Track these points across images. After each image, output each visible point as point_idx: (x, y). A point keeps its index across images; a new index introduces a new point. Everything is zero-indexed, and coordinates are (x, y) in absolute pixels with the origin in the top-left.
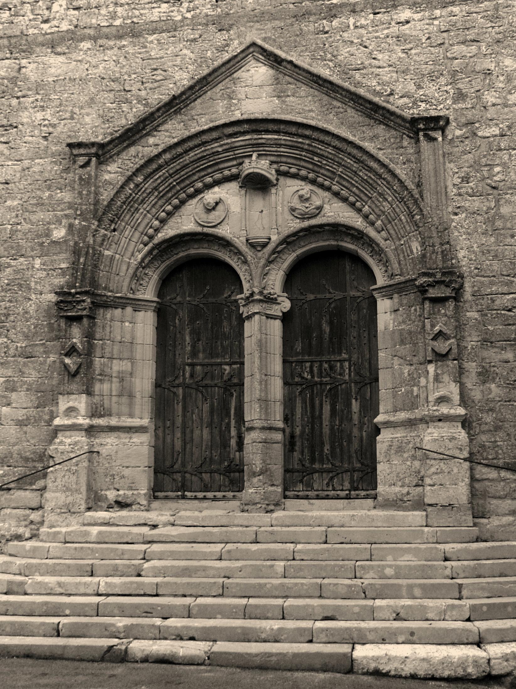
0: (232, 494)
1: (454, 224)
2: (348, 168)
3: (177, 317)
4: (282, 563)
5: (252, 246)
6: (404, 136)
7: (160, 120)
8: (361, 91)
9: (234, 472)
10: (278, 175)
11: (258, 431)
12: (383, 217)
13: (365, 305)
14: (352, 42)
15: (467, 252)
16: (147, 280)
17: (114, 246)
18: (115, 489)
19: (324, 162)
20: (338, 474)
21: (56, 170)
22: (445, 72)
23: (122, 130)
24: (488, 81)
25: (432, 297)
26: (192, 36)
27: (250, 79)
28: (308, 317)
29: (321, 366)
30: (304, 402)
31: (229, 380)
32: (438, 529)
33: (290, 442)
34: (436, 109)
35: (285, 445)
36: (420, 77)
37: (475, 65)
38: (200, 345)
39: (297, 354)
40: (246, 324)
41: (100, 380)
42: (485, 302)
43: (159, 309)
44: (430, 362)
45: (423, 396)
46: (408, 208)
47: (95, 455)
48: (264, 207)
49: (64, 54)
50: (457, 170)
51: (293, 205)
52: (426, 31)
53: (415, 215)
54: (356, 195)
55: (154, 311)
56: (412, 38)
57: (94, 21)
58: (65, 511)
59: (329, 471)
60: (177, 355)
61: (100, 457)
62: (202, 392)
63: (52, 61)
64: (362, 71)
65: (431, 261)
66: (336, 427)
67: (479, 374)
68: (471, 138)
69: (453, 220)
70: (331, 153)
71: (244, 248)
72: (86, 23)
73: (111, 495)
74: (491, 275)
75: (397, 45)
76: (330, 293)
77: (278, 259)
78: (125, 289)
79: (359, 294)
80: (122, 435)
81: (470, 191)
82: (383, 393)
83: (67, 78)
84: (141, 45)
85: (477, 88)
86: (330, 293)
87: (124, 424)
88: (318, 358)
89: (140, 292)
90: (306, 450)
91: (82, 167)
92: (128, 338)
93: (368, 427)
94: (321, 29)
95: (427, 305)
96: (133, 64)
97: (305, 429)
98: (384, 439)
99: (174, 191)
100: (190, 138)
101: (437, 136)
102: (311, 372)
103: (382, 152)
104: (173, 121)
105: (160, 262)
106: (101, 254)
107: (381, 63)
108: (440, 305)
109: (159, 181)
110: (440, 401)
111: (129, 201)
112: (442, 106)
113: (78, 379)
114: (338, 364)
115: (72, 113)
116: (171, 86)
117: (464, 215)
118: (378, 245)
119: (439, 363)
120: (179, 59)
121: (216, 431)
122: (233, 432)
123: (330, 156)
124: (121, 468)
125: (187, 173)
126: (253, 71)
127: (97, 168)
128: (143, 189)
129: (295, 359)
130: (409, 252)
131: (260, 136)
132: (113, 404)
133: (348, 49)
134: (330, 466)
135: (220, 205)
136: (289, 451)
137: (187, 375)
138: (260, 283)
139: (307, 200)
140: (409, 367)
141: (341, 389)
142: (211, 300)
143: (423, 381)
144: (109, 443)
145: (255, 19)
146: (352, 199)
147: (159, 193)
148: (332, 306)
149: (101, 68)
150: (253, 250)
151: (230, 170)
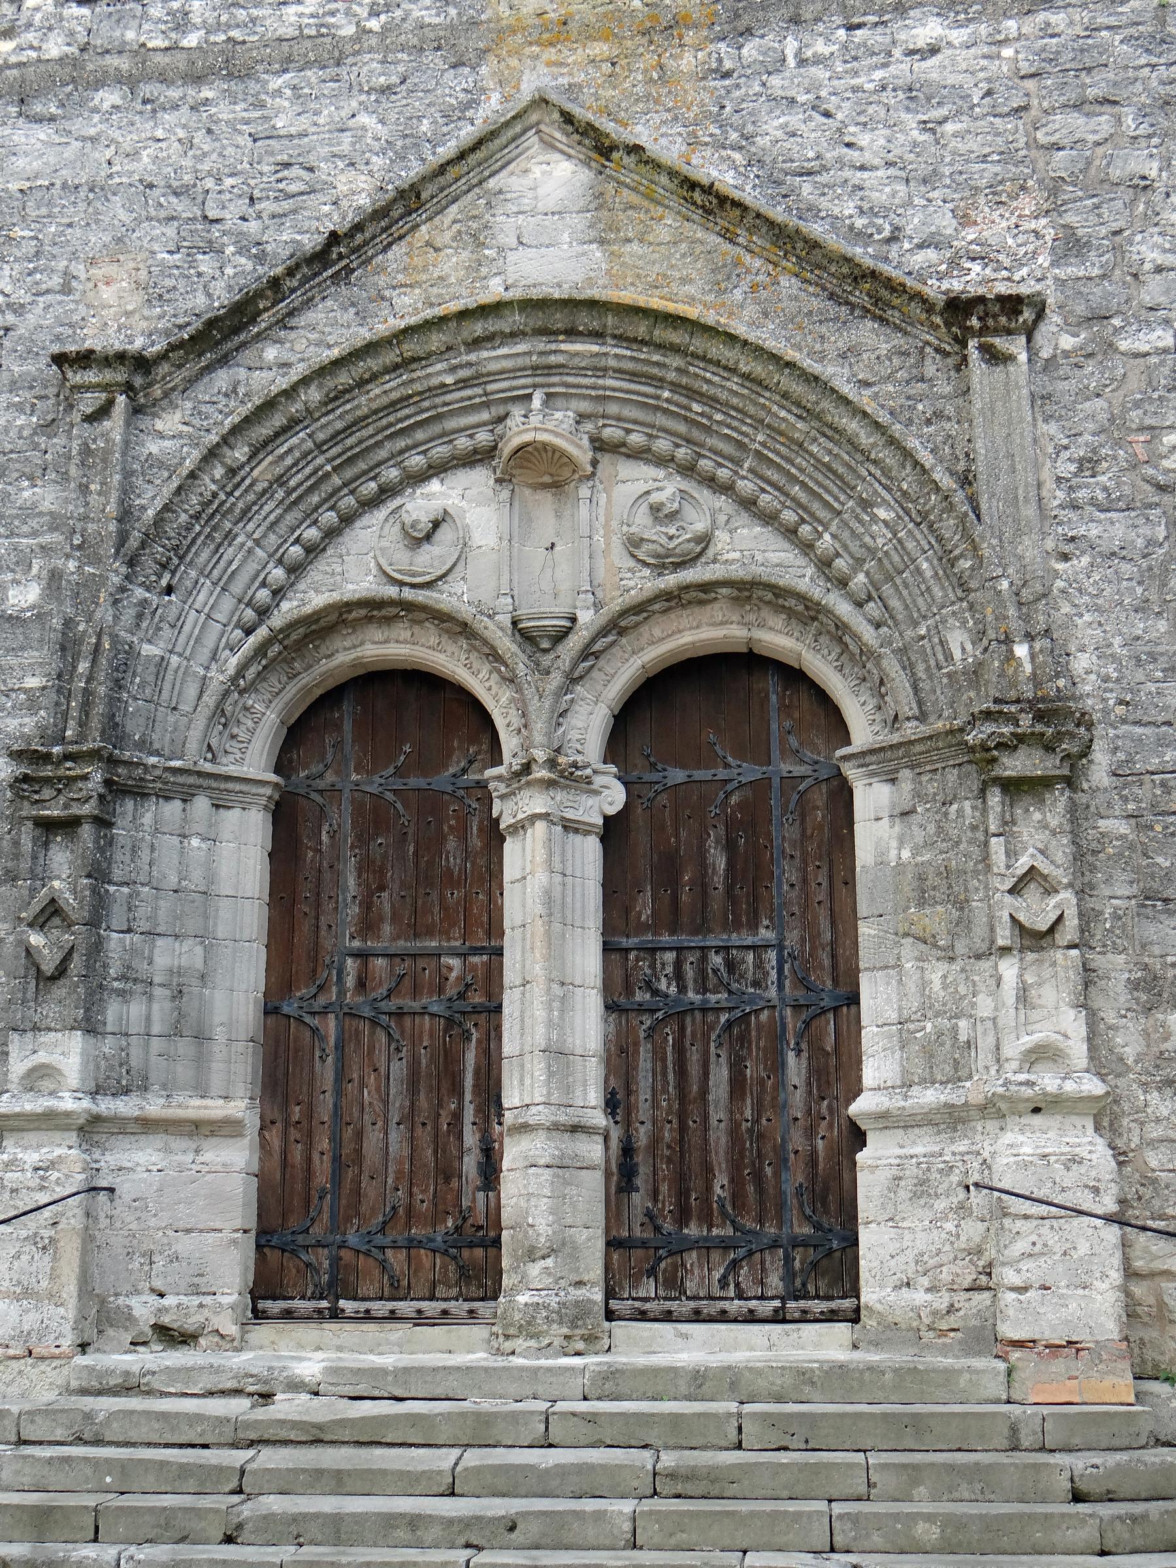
0: (467, 1306)
1: (1060, 584)
2: (781, 433)
3: (325, 828)
4: (627, 1506)
5: (525, 636)
6: (928, 350)
7: (296, 299)
8: (816, 229)
9: (471, 1245)
10: (595, 449)
11: (542, 1134)
12: (870, 565)
13: (819, 797)
14: (792, 101)
15: (1094, 658)
16: (250, 723)
17: (167, 632)
18: (153, 1290)
19: (718, 417)
20: (751, 1253)
21: (22, 428)
22: (1030, 183)
23: (198, 324)
24: (1141, 207)
25: (1009, 779)
26: (382, 79)
27: (530, 194)
28: (670, 830)
29: (704, 959)
30: (658, 1055)
31: (461, 996)
32: (1046, 1410)
33: (620, 1166)
34: (1009, 279)
35: (608, 1175)
36: (967, 194)
37: (1109, 164)
38: (385, 902)
39: (642, 928)
40: (510, 847)
41: (121, 993)
42: (1146, 792)
43: (277, 804)
44: (1005, 950)
45: (986, 1043)
46: (940, 539)
47: (102, 1197)
48: (558, 534)
49: (52, 119)
50: (1065, 442)
51: (633, 529)
52: (982, 75)
53: (957, 558)
54: (800, 505)
55: (266, 808)
56: (945, 92)
57: (130, 35)
58: (18, 1352)
59: (725, 1245)
60: (324, 928)
61: (118, 1202)
62: (386, 1029)
63: (18, 137)
64: (818, 179)
65: (1004, 683)
66: (744, 1125)
67: (1134, 986)
68: (1100, 357)
69: (1056, 574)
70: (736, 393)
71: (506, 644)
72: (111, 40)
73: (143, 1308)
74: (1160, 719)
75: (908, 109)
76: (727, 766)
77: (595, 674)
78: (193, 746)
79: (799, 770)
80: (177, 1143)
81: (1101, 496)
82: (871, 1037)
83: (58, 183)
84: (251, 100)
85: (1115, 226)
86: (727, 766)
87: (181, 1113)
88: (696, 941)
89: (231, 758)
90: (664, 1188)
91: (90, 419)
92: (196, 880)
93: (831, 1126)
94: (714, 65)
95: (995, 798)
96: (230, 151)
97: (662, 1129)
98: (876, 1163)
99: (327, 488)
100: (370, 348)
101: (1013, 349)
102: (679, 975)
103: (867, 392)
104: (329, 303)
105: (284, 679)
106: (131, 652)
107: (867, 157)
108: (1027, 799)
109: (289, 461)
110: (1034, 1056)
111: (210, 513)
112: (1024, 271)
113: (60, 990)
114: (750, 957)
115: (68, 277)
116: (327, 208)
117: (1085, 560)
118: (856, 637)
119: (1030, 956)
120: (347, 138)
121: (424, 1136)
122: (471, 1138)
123: (735, 401)
124: (170, 1233)
125: (360, 442)
126: (537, 171)
127: (128, 424)
128: (248, 482)
129: (633, 941)
130: (941, 657)
131: (553, 347)
132: (153, 1059)
133: (781, 120)
134: (730, 1232)
135: (444, 529)
136: (620, 1190)
137: (350, 981)
138: (548, 735)
139: (673, 516)
140: (943, 967)
141: (759, 1027)
142: (415, 782)
143: (984, 1006)
144: (139, 1163)
145: (545, 36)
146: (789, 516)
147: (289, 493)
148: (734, 800)
149: (146, 160)
150: (529, 649)
151: (471, 436)
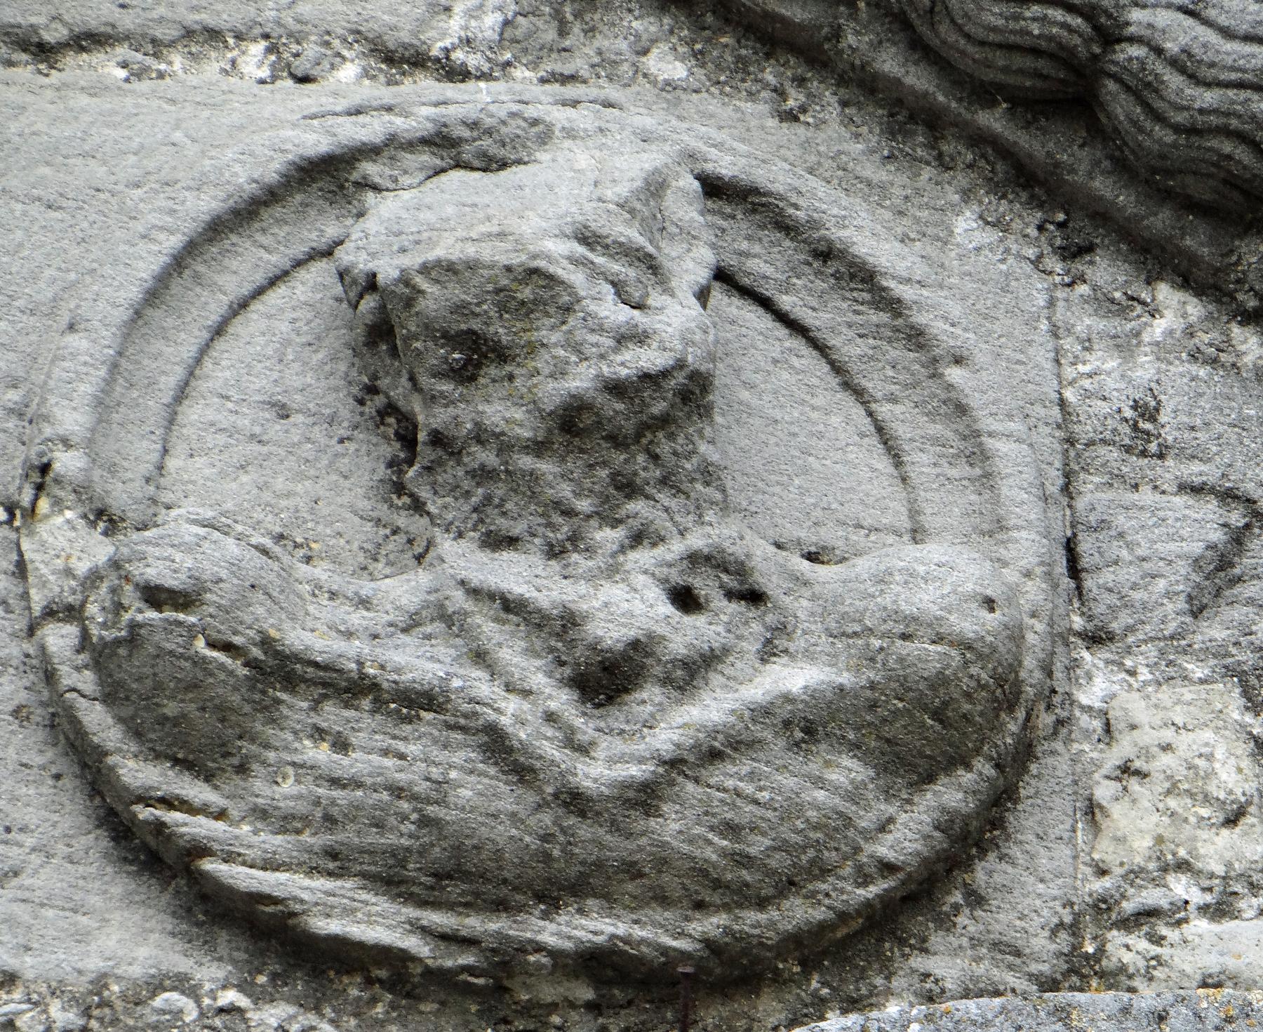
139: (643, 432)
